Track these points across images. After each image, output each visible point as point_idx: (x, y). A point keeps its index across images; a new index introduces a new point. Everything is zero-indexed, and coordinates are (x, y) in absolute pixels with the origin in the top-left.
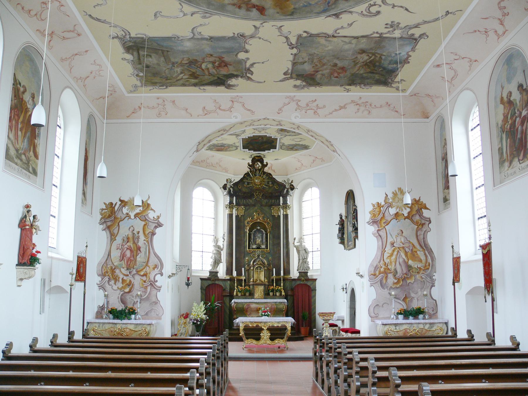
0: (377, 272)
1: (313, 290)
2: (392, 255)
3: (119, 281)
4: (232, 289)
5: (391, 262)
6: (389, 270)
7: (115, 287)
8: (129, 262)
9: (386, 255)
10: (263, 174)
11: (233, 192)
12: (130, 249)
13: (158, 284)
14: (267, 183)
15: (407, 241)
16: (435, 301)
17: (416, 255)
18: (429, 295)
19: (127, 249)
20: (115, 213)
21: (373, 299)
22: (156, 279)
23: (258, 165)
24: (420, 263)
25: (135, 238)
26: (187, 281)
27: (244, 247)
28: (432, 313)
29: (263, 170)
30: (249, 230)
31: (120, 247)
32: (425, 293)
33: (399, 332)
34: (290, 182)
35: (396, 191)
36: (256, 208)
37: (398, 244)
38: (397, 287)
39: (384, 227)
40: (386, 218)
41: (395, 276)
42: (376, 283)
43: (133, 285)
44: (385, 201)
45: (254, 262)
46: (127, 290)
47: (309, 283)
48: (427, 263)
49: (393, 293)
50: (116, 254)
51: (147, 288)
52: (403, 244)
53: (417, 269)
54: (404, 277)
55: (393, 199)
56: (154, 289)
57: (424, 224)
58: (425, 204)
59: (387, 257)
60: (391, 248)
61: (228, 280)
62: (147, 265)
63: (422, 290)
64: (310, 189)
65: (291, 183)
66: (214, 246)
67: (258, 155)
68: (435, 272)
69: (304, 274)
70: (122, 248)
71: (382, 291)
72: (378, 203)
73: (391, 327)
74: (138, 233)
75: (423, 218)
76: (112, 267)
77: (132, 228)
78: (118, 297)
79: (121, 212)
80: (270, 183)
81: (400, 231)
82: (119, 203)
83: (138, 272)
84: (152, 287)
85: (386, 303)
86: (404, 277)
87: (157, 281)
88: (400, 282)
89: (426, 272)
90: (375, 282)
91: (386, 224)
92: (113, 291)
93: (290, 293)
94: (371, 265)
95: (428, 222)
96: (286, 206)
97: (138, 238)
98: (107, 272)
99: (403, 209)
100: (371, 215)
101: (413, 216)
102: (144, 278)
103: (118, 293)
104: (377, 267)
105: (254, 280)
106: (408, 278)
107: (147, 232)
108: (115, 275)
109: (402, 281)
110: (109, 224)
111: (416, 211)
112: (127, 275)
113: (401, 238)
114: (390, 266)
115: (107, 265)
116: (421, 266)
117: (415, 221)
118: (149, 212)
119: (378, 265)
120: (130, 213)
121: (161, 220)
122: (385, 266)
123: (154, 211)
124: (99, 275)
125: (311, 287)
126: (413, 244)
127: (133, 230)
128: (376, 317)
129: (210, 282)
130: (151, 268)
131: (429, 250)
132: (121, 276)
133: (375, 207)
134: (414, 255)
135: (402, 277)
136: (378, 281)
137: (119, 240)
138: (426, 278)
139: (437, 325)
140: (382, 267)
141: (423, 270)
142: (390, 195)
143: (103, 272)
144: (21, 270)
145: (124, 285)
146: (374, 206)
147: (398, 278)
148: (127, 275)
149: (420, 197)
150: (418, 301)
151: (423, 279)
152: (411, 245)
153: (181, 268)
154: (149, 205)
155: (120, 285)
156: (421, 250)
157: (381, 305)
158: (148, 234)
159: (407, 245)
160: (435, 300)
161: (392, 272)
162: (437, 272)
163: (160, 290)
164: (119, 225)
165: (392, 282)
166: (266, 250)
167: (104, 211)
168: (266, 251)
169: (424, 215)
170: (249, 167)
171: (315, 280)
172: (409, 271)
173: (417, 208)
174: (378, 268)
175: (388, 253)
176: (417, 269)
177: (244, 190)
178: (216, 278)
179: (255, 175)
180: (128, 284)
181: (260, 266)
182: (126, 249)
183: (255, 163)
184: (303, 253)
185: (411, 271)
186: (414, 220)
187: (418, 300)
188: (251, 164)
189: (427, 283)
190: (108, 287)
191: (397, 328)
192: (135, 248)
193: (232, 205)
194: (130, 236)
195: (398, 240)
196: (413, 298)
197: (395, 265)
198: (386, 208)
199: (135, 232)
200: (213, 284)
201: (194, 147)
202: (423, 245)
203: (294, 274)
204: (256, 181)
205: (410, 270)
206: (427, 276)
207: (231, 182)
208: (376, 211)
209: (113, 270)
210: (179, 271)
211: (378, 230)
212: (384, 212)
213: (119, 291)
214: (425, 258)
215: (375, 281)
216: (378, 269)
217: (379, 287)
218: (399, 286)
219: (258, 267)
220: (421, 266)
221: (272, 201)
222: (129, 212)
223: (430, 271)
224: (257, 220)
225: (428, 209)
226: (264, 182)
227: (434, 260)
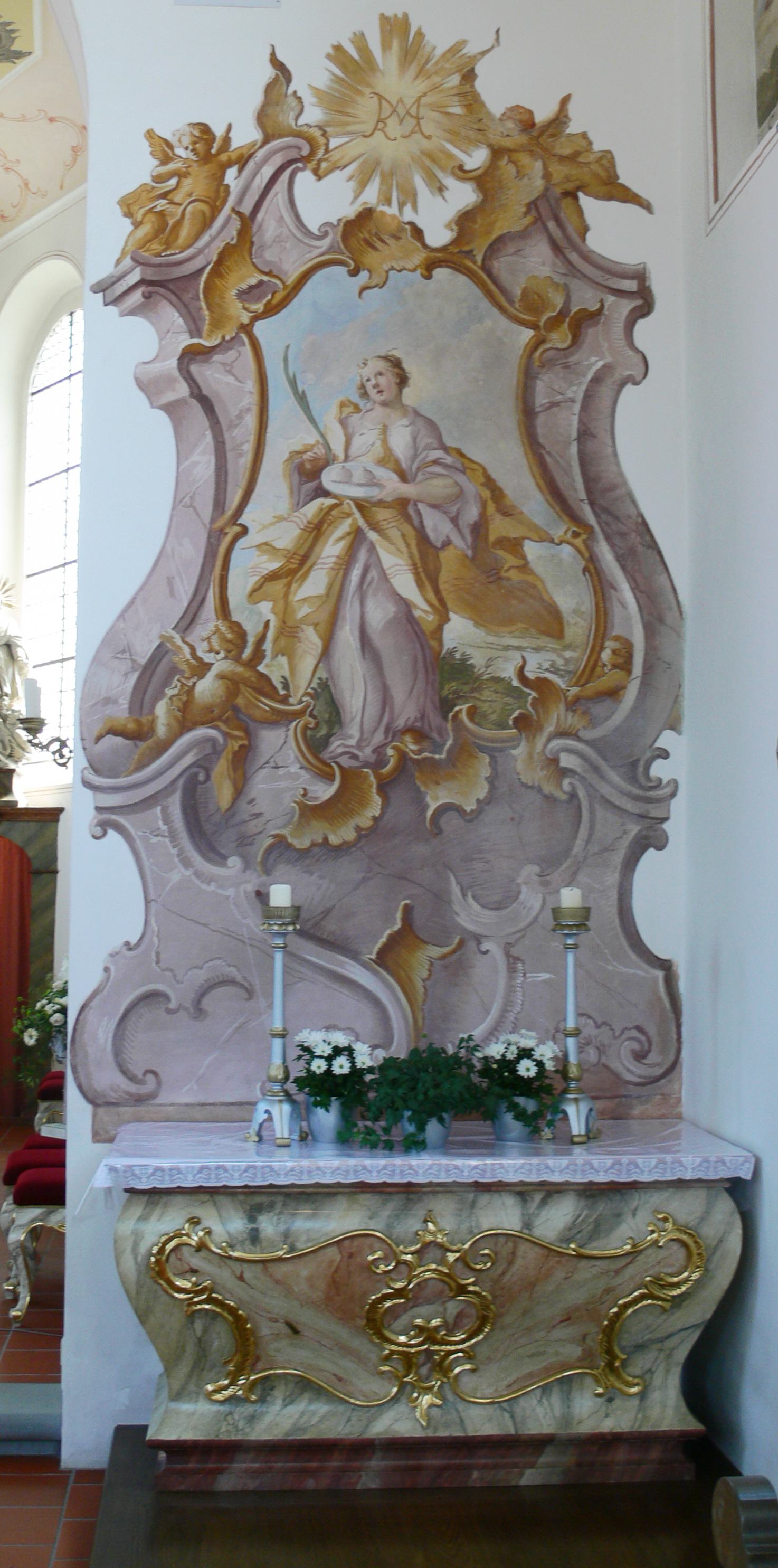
0: (161, 709)
1: (38, 873)
15: (438, 454)
16: (660, 974)
17: (514, 575)
18: (607, 909)
21: (116, 943)
24: (544, 641)
28: (631, 1070)
32: (570, 898)
33: (284, 1268)
35: (360, 40)
37: (358, 476)
38: (334, 840)
39: (246, 328)
44: (262, 117)
48: (610, 644)
49: (280, 896)
52: (403, 477)
53: (516, 694)
54: (403, 756)
57: (593, 316)
58: (607, 159)
59: (252, 581)
60: (298, 505)
63: (555, 876)
68: (674, 725)
71: (198, 874)
72: (205, 129)
73: (210, 1219)
81: (382, 365)
85: (232, 982)
86: (403, 756)
88: (364, 803)
89: (593, 723)
91: (259, 307)
95: (627, 306)
100: (137, 225)
101: (495, 248)
106: (433, 765)
109: (383, 789)
111: (532, 206)
113: (385, 430)
114: (283, 660)
116: (555, 670)
117: (518, 292)
122: (237, 659)
125: (31, 853)
126: (489, 482)
128: (139, 1100)
131: (623, 535)
133: (171, 166)
134: (494, 574)
135: (380, 762)
138: (596, 769)
139: (656, 1199)
140: (202, 668)
141: (573, 705)
147: (345, 762)
149: (565, 101)
150: (512, 970)
151: (566, 783)
152: (471, 487)
156: (560, 530)
159: (439, 487)
160: (666, 966)
162: (686, 724)
165: (289, 803)
169: (594, 242)
172: (445, 706)
173: (539, 183)
174: (174, 670)
175: (266, 547)
176: (516, 694)
185: (463, 708)
186: (505, 277)
187: (512, 961)
189: (600, 812)
191: (268, 1225)
195: (357, 442)
196: (472, 945)
197: (326, 653)
202: (577, 489)
205: (459, 697)
206: (599, 752)
208: (178, 198)
211: (190, 355)
212: (246, 208)
214: (588, 604)
216: (166, 683)
217: (173, 836)
220: (555, 670)
223: (635, 709)
225: (627, 196)
227: (670, 617)
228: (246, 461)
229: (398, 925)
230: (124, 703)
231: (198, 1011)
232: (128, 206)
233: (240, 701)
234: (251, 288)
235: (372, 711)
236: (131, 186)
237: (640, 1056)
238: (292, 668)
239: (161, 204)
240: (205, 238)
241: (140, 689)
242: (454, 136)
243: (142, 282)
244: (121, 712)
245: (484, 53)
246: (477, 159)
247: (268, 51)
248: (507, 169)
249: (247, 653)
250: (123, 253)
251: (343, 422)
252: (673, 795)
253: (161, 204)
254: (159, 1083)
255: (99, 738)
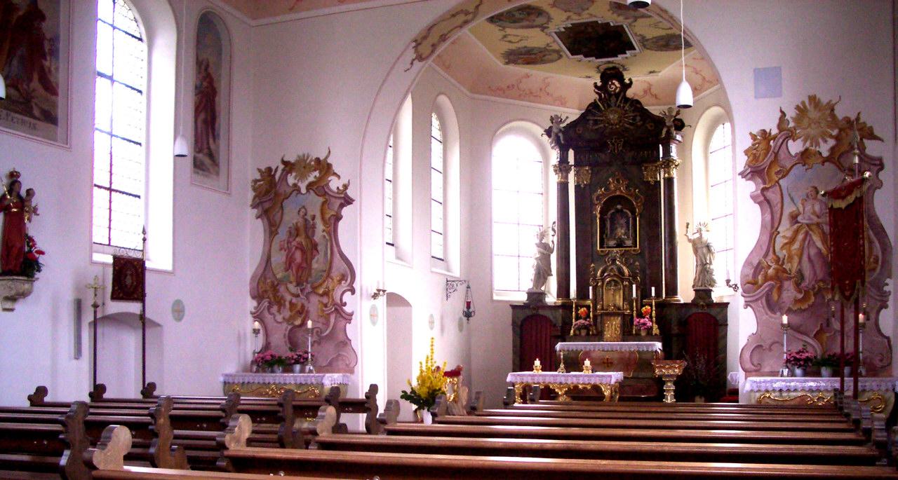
0: (760, 277)
2: (792, 240)
3: (285, 305)
4: (567, 324)
5: (790, 258)
6: (787, 273)
7: (279, 318)
8: (300, 272)
9: (780, 241)
10: (624, 103)
11: (564, 140)
12: (300, 247)
13: (347, 309)
14: (633, 119)
16: (886, 340)
19: (297, 248)
20: (275, 185)
21: (750, 333)
22: (344, 301)
23: (612, 86)
25: (308, 228)
26: (466, 310)
27: (592, 245)
28: (879, 364)
29: (625, 94)
30: (600, 213)
31: (286, 246)
34: (674, 114)
35: (803, 103)
36: (613, 169)
37: (807, 217)
38: (803, 308)
39: (777, 182)
40: (782, 162)
41: (798, 285)
42: (757, 300)
43: (308, 312)
44: (779, 126)
45: (603, 272)
46: (298, 322)
47: (713, 312)
48: (873, 257)
50: (279, 258)
51: (330, 317)
52: (818, 217)
54: (819, 287)
55: (798, 120)
56: (341, 319)
58: (871, 129)
59: (782, 245)
60: (792, 226)
61: (558, 307)
62: (328, 276)
64: (721, 126)
65: (676, 116)
66: (536, 244)
67: (611, 65)
68: (890, 277)
69: (703, 293)
70: (288, 247)
71: (770, 317)
72: (764, 131)
74: (314, 218)
75: (866, 160)
76: (273, 282)
77: (303, 210)
78: (285, 335)
79: (284, 183)
80: (638, 118)
81: (812, 189)
82: (281, 167)
83: (314, 289)
84: (338, 315)
86: (819, 287)
87: (345, 304)
88: (810, 298)
90: (754, 298)
91: (780, 176)
92: (275, 324)
93: (675, 330)
94: (748, 263)
96: (668, 163)
97: (314, 227)
98: (266, 291)
99: (820, 140)
100: (749, 157)
101: (840, 156)
102: (325, 300)
103: (285, 327)
104: (760, 267)
105: (603, 305)
107: (327, 216)
108: (278, 297)
109: (815, 295)
110: (267, 205)
112: (298, 296)
114: (790, 264)
115: (265, 279)
118: (329, 179)
119: (763, 263)
120: (300, 184)
121: (350, 192)
123: (339, 177)
124: (254, 297)
127: (306, 215)
129: (528, 312)
130: (335, 281)
132: (288, 298)
136: (761, 298)
137: (283, 234)
140: (769, 267)
142: (791, 114)
143: (260, 291)
144: (4, 282)
145: (294, 312)
146: (754, 137)
148: (298, 296)
149: (859, 114)
153: (455, 286)
154: (329, 166)
155: (287, 313)
157: (766, 346)
158: (329, 218)
160: (888, 338)
161: (794, 277)
163: (350, 320)
164: (282, 204)
166: (633, 248)
167: (259, 183)
168: (634, 250)
170: (596, 91)
171: (726, 305)
174: (763, 268)
175: (784, 237)
177: (588, 136)
178: (540, 304)
179: (609, 106)
180: (299, 311)
181: (615, 279)
182: (294, 249)
183: (607, 83)
184: (702, 250)
186: (844, 164)
188: (599, 84)
190: (268, 318)
192: (309, 246)
193: (565, 165)
194: (301, 224)
195: (806, 209)
197: (800, 262)
198: (781, 140)
199: (309, 218)
200: (532, 316)
201: (405, 50)
203: (685, 294)
204: (611, 117)
207: (561, 121)
209: (275, 288)
210: (451, 291)
211: (763, 190)
212: (776, 151)
213: (285, 325)
215: (754, 296)
217: (763, 308)
218: (807, 306)
219: (610, 281)
221: (643, 153)
222: (298, 181)
224: (615, 191)
226: (627, 117)
228: (778, 216)
229: (819, 328)
230: (751, 276)
231: (770, 350)
232: (746, 152)
233: (779, 274)
234: (778, 171)
235: (812, 276)
236: (747, 147)
237: (881, 361)
238: (792, 266)
239: (755, 152)
240: (766, 159)
241: (755, 272)
242: (829, 127)
243: (751, 172)
244: (750, 278)
245: (836, 103)
246: (835, 132)
247: (779, 109)
248: (844, 134)
249: (780, 263)
250: (746, 164)
251: (803, 204)
252: (890, 294)
253: (755, 152)
254: (306, 210)
255: (745, 285)
